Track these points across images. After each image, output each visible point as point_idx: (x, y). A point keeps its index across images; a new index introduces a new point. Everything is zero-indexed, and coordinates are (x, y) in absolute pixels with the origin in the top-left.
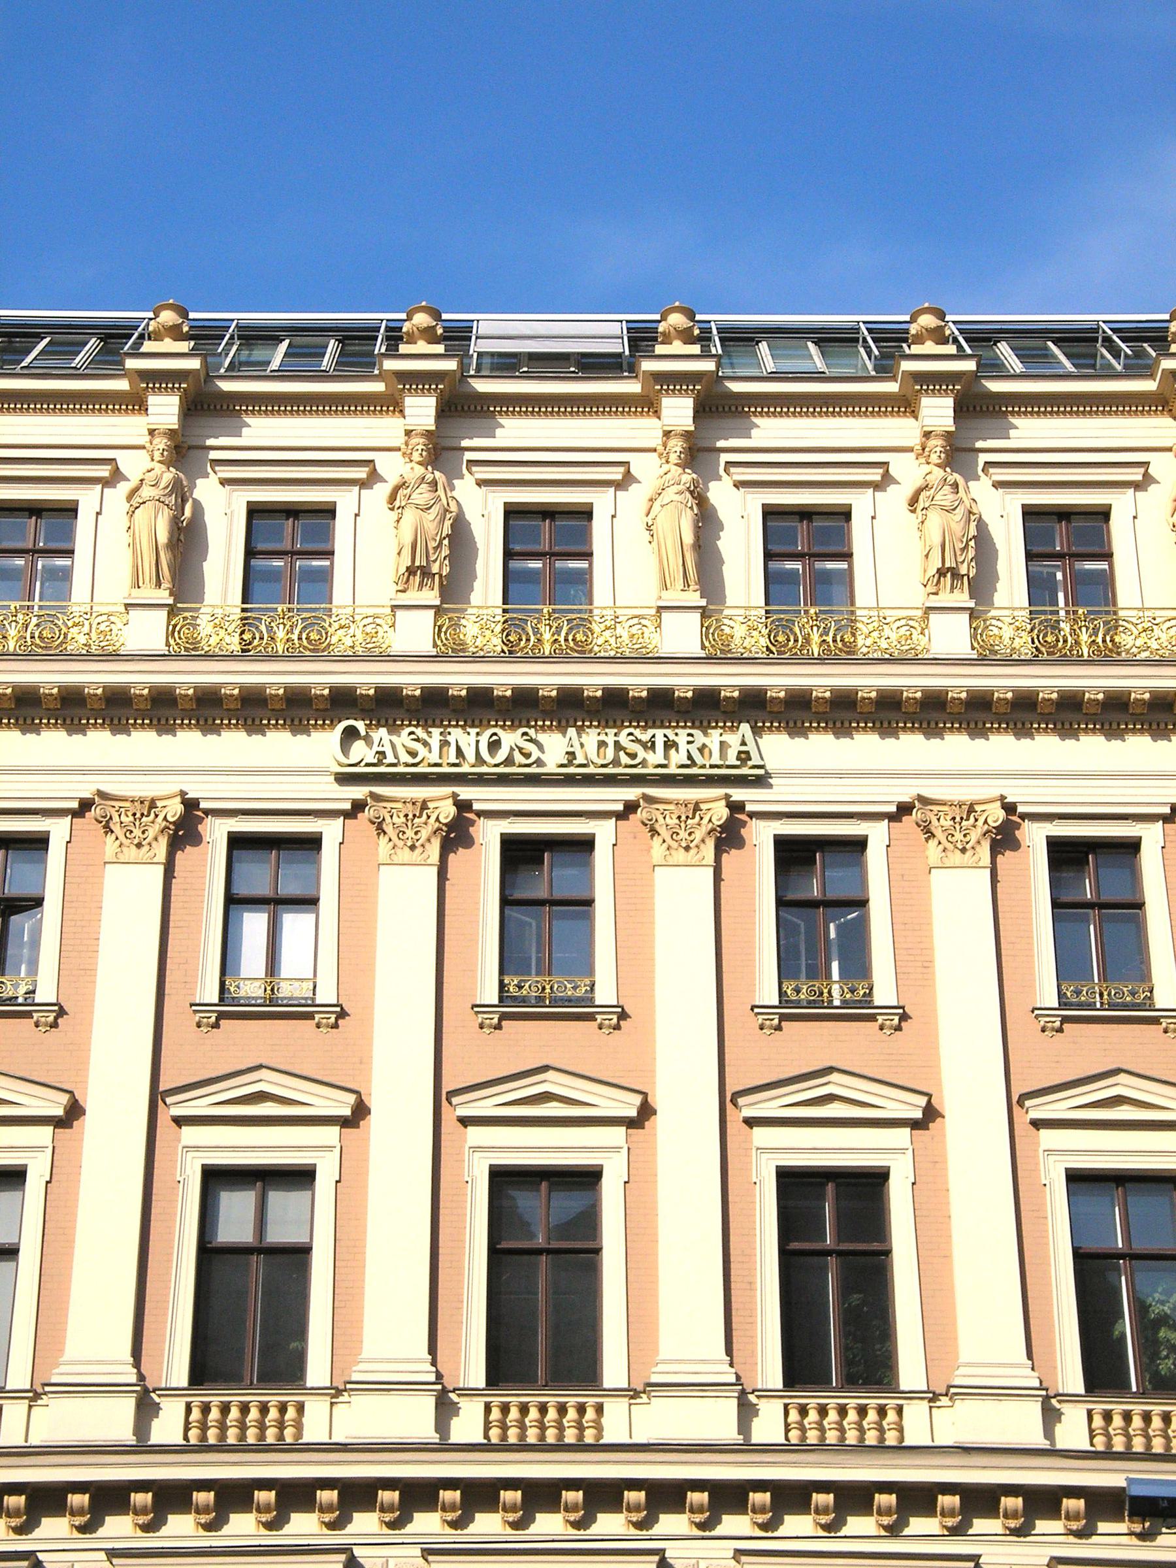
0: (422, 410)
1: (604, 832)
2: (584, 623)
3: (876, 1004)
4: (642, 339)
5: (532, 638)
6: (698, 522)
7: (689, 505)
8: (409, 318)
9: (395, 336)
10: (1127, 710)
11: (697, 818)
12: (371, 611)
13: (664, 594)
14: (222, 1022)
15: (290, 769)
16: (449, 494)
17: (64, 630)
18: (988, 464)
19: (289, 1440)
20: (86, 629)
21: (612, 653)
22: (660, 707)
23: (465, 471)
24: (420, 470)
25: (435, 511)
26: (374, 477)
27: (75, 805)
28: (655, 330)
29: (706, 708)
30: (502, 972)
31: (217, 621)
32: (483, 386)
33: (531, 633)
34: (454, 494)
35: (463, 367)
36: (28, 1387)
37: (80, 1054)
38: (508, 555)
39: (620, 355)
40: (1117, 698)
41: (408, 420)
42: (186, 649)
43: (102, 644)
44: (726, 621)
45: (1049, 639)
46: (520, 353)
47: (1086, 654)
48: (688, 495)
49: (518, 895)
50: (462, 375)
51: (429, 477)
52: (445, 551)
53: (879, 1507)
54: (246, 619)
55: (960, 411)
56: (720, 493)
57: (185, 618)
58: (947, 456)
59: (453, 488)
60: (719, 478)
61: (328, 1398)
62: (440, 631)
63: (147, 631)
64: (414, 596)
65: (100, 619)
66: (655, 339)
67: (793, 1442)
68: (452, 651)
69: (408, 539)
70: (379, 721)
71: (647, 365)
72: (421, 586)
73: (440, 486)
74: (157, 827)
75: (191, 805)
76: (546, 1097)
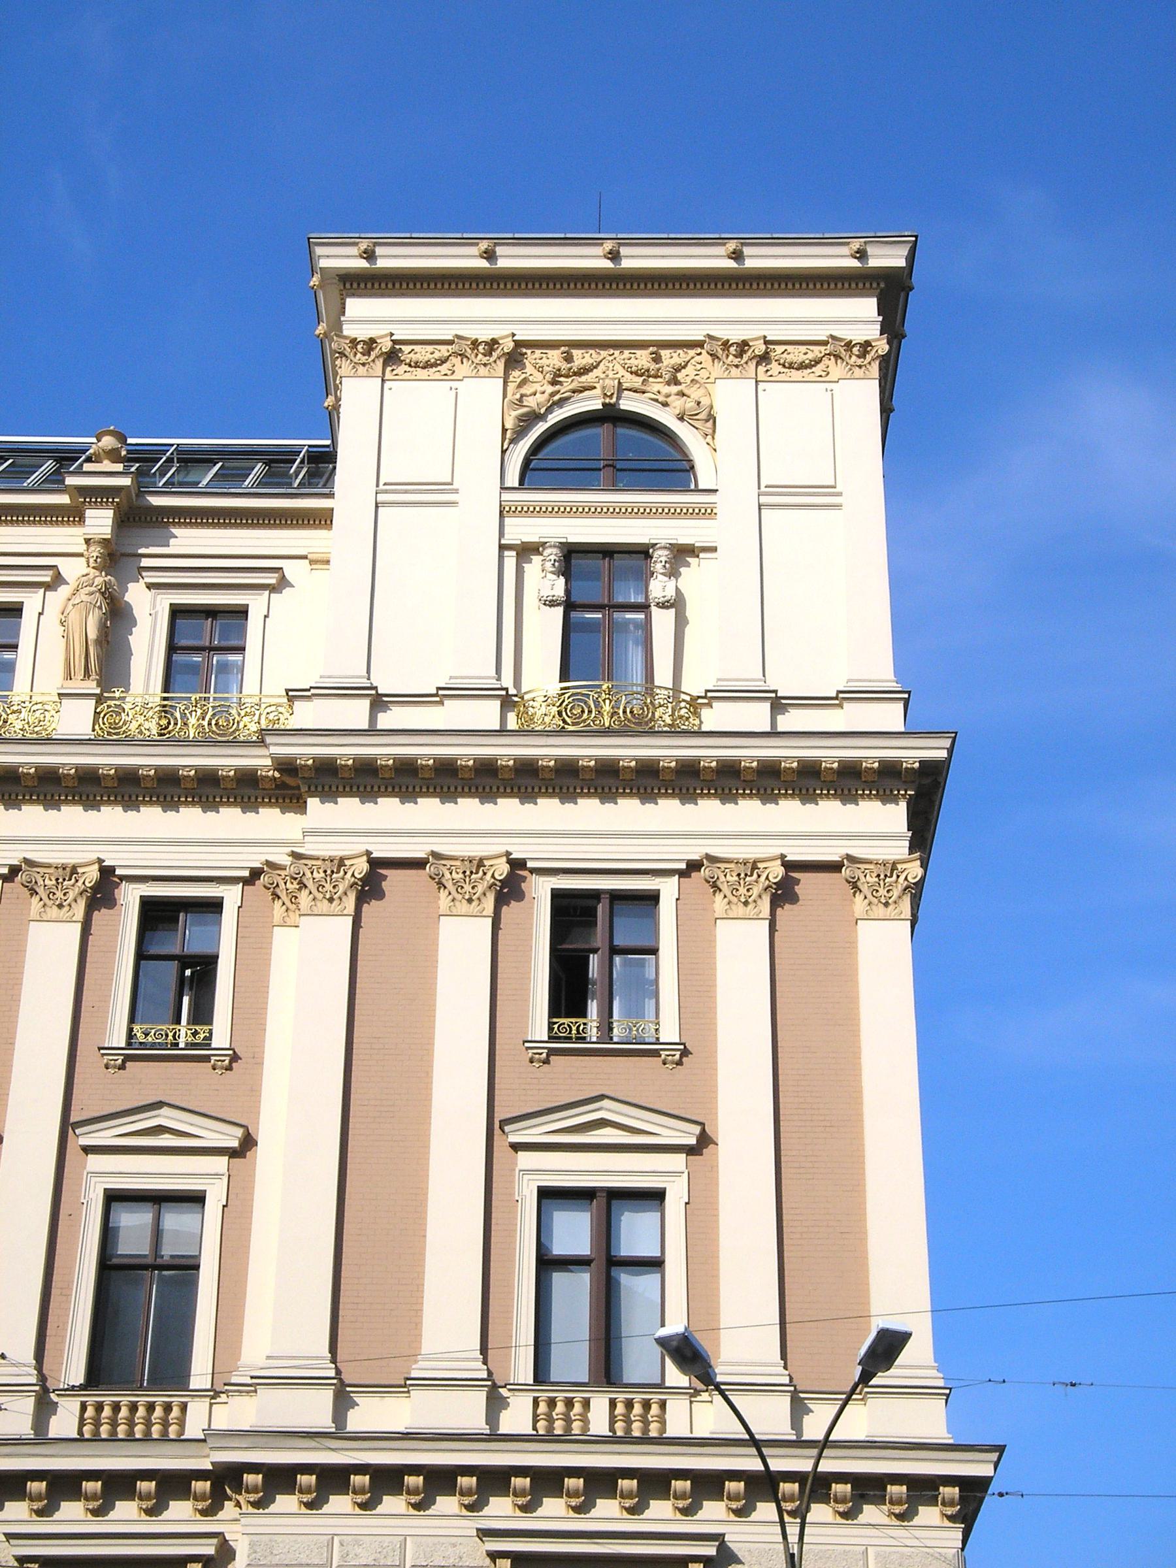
0: (101, 521)
3: (213, 1046)
6: (106, 620)
10: (699, 776)
11: (755, 875)
14: (552, 1058)
17: (238, 718)
19: (620, 1433)
20: (256, 718)
26: (58, 580)
27: (246, 873)
30: (132, 1019)
31: (138, 709)
36: (209, 1387)
37: (254, 1091)
40: (850, 767)
42: (109, 734)
47: (192, 736)
49: (154, 950)
53: (729, 1493)
54: (164, 706)
56: (137, 595)
57: (109, 707)
61: (208, 1399)
63: (77, 719)
65: (269, 710)
67: (541, 1432)
71: (70, 481)
74: (900, 888)
76: (160, 1130)
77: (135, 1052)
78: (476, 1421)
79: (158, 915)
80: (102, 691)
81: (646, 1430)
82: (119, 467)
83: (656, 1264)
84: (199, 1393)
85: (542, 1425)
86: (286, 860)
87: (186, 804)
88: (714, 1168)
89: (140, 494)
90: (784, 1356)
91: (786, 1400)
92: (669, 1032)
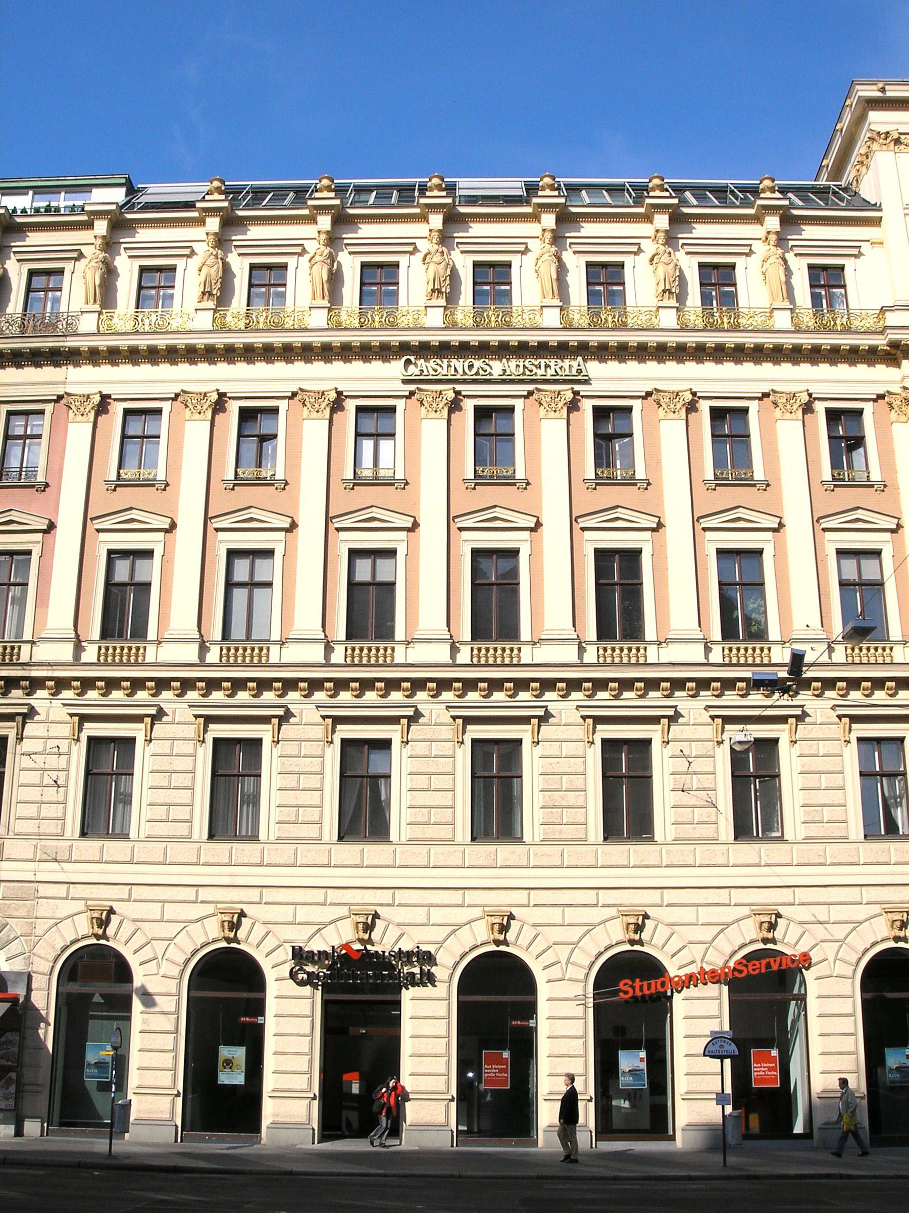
0: (436, 220)
1: (519, 404)
2: (509, 313)
4: (532, 189)
9: (423, 189)
13: (544, 300)
15: (383, 378)
22: (543, 350)
24: (436, 247)
26: (416, 250)
27: (290, 394)
29: (563, 350)
30: (237, 467)
32: (463, 210)
35: (454, 201)
38: (475, 283)
49: (482, 432)
50: (454, 205)
51: (440, 250)
52: (448, 282)
55: (558, 221)
63: (319, 319)
64: (435, 302)
68: (452, 326)
71: (535, 200)
74: (90, 407)
75: (339, 394)
76: (858, 520)
77: (238, 482)
78: (573, 658)
79: (247, 415)
81: (487, 661)
82: (223, 197)
83: (269, 585)
84: (651, 643)
85: (224, 659)
86: (899, 391)
87: (841, 362)
88: (296, 538)
89: (233, 210)
90: (574, 626)
91: (322, 646)
92: (161, 476)
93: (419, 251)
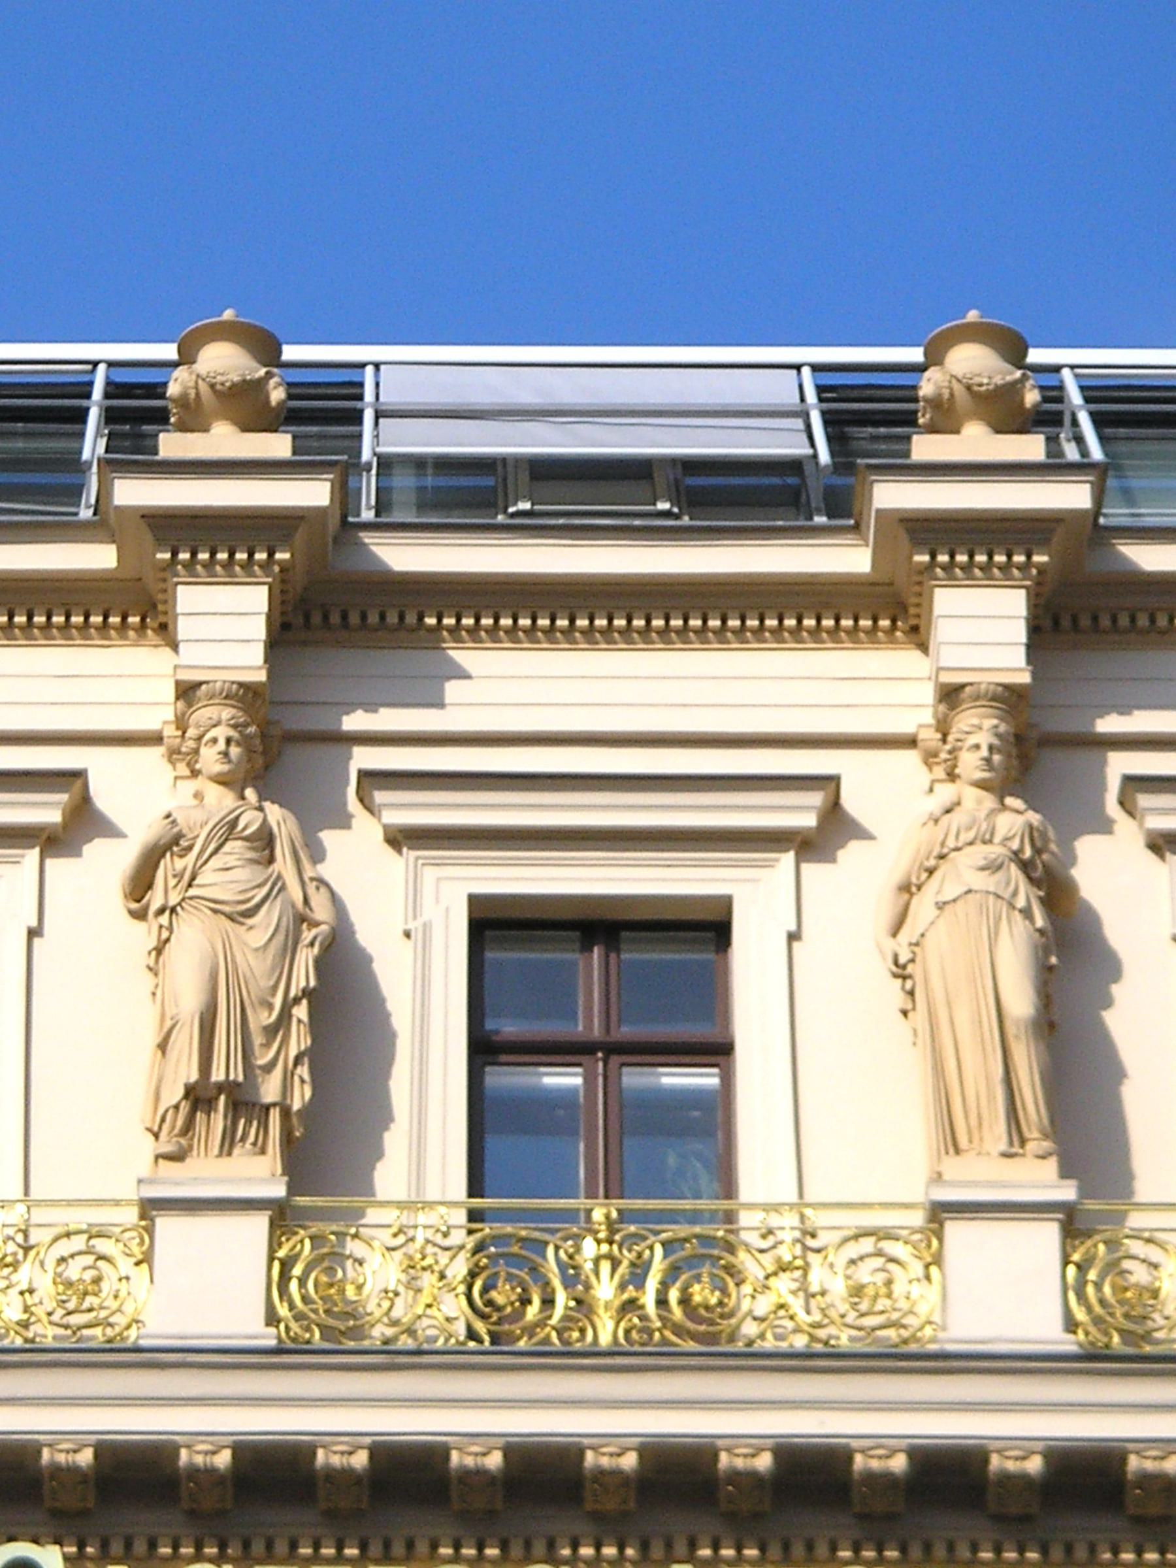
0: (227, 624)
2: (713, 1254)
4: (870, 418)
5: (562, 1299)
6: (1047, 952)
7: (1021, 902)
8: (187, 357)
9: (139, 413)
12: (80, 1218)
13: (952, 1167)
16: (309, 872)
18: (1135, 783)
21: (800, 1342)
23: (353, 803)
24: (220, 800)
25: (268, 919)
26: (83, 823)
28: (910, 394)
32: (405, 556)
33: (557, 1283)
34: (325, 870)
35: (345, 496)
38: (483, 1049)
39: (794, 466)
41: (189, 654)
43: (75, 1320)
44: (1136, 1247)
45: (498, 1297)
46: (504, 460)
48: (1014, 870)
50: (343, 523)
51: (250, 821)
52: (298, 1040)
55: (1048, 629)
58: (249, 751)
59: (318, 855)
60: (1105, 826)
62: (285, 1277)
64: (209, 1173)
66: (909, 419)
68: (324, 1337)
69: (188, 1002)
70: (105, 1545)
71: (891, 495)
72: (229, 1143)
73: (282, 850)
80: (292, 1190)
93: (108, 830)
